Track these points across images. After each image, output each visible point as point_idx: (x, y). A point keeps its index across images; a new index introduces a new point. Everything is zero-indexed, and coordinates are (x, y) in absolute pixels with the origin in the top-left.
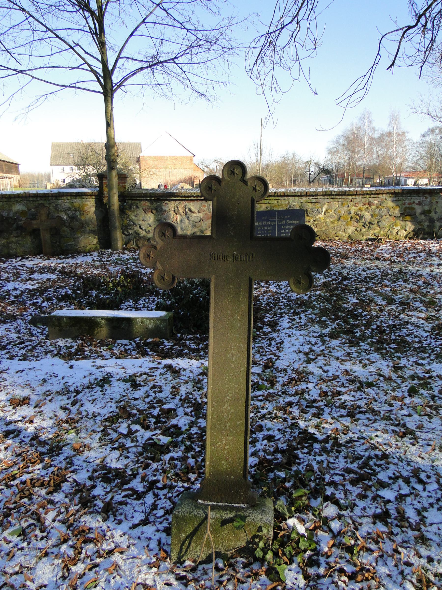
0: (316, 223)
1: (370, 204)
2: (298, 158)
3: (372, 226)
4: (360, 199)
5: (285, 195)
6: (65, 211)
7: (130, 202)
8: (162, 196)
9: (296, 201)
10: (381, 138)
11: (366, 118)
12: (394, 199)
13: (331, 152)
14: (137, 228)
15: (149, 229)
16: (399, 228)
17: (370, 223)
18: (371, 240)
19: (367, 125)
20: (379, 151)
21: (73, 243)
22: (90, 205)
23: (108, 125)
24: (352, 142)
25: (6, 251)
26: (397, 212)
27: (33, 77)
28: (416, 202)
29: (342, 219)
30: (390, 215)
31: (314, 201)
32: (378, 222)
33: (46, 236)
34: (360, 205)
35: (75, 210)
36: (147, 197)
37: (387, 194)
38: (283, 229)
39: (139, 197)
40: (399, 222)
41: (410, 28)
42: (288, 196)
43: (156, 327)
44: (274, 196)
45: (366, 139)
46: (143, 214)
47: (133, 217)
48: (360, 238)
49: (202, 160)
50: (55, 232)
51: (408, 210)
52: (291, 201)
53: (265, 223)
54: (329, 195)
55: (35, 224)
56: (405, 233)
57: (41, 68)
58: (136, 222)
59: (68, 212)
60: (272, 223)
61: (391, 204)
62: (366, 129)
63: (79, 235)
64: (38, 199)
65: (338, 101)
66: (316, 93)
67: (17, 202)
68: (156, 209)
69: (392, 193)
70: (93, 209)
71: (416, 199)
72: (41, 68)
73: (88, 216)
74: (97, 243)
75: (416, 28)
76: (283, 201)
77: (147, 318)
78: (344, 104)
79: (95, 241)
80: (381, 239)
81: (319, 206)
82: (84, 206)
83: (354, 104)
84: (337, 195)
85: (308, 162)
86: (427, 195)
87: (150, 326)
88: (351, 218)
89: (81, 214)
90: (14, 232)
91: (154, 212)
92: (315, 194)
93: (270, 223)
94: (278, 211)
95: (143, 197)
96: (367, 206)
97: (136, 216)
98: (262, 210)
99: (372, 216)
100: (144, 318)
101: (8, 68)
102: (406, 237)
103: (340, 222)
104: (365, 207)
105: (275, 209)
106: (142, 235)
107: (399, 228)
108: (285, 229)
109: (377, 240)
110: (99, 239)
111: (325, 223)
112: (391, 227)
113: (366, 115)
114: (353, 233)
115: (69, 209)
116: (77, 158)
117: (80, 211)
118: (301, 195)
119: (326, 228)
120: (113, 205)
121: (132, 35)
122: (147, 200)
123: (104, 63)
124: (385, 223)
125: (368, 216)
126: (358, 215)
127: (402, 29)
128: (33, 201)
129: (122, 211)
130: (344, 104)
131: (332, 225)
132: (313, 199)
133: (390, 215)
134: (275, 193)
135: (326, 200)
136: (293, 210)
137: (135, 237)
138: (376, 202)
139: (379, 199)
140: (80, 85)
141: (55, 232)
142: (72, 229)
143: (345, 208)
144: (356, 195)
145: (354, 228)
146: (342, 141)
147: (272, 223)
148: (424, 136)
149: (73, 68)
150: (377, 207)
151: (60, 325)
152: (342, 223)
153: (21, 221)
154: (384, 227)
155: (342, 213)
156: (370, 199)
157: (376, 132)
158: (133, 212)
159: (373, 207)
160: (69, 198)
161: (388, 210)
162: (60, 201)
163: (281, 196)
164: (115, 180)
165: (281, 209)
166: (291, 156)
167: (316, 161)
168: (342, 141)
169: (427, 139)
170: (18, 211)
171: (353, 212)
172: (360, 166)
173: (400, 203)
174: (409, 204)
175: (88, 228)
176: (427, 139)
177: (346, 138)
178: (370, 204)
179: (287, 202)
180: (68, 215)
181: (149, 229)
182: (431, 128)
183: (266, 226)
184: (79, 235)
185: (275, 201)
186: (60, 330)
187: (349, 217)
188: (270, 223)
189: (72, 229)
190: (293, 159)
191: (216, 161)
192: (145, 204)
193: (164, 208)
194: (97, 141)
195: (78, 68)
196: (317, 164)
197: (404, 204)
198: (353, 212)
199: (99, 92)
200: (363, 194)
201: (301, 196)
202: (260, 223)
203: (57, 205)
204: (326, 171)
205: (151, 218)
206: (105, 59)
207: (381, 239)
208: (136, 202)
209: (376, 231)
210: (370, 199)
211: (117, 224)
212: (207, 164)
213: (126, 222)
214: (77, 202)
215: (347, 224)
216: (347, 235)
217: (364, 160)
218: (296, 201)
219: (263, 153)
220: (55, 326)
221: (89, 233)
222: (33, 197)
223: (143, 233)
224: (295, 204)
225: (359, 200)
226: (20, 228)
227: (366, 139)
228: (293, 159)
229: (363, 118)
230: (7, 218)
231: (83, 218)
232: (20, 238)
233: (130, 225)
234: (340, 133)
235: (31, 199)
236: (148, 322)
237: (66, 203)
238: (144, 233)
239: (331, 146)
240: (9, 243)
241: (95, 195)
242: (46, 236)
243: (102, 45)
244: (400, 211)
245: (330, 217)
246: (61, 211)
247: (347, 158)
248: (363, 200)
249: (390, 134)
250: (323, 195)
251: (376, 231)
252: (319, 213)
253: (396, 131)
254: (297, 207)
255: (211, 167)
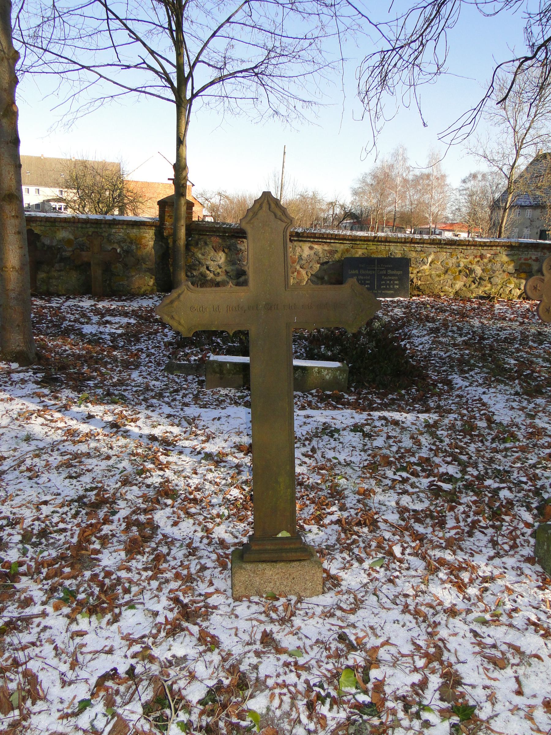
0: (419, 275)
1: (482, 257)
2: (319, 197)
3: (483, 283)
4: (471, 251)
5: (386, 240)
6: (119, 243)
7: (197, 237)
8: (238, 233)
9: (399, 248)
10: (417, 180)
11: (400, 155)
12: (510, 253)
13: (356, 193)
14: (203, 269)
15: (219, 270)
16: (512, 286)
17: (480, 278)
18: (482, 298)
19: (401, 163)
20: (412, 195)
21: (126, 283)
22: (149, 237)
23: (180, 142)
24: (382, 182)
25: (45, 288)
26: (511, 268)
27: (101, 76)
28: (534, 257)
29: (449, 272)
30: (504, 271)
31: (419, 249)
32: (489, 278)
33: (97, 272)
34: (471, 258)
35: (131, 243)
36: (219, 232)
37: (502, 246)
38: (383, 280)
39: (209, 231)
40: (513, 280)
41: (527, 59)
42: (390, 242)
43: (335, 378)
44: (373, 241)
45: (399, 180)
46: (212, 253)
47: (200, 256)
48: (469, 295)
49: (201, 191)
50: (107, 268)
51: (524, 267)
52: (392, 248)
53: (362, 272)
54: (437, 244)
55: (85, 256)
56: (519, 292)
57: (108, 65)
58: (203, 261)
59: (122, 245)
60: (370, 272)
61: (505, 259)
62: (399, 169)
63: (133, 274)
64: (88, 226)
65: (440, 136)
66: (424, 125)
67: (63, 227)
68: (229, 248)
69: (508, 246)
70: (151, 243)
71: (534, 254)
72: (108, 65)
73: (146, 250)
74: (154, 285)
75: (534, 60)
76: (383, 247)
77: (325, 368)
78: (448, 139)
79: (151, 282)
80: (494, 298)
81: (424, 255)
82: (142, 238)
83: (459, 140)
84: (445, 244)
85: (332, 203)
86: (545, 251)
87: (328, 377)
88: (460, 272)
89: (137, 248)
90: (57, 265)
91: (226, 250)
92: (422, 242)
93: (368, 272)
94: (378, 258)
95: (214, 232)
96: (478, 259)
97: (203, 255)
98: (357, 256)
99: (483, 270)
100: (322, 368)
101: (75, 63)
102: (519, 297)
103: (447, 276)
104: (476, 260)
105: (374, 256)
106: (209, 278)
107: (512, 286)
108: (385, 280)
109: (488, 297)
110: (156, 279)
111: (430, 275)
112: (505, 284)
113: (401, 151)
114: (460, 289)
115: (124, 241)
116: (64, 177)
117: (137, 245)
118: (405, 241)
119: (431, 281)
120: (180, 239)
121: (213, 35)
122: (219, 236)
123: (179, 67)
124: (498, 280)
125: (479, 271)
126: (468, 268)
127: (519, 59)
128: (82, 228)
129: (188, 246)
130: (448, 139)
131: (438, 279)
132: (418, 247)
133: (504, 271)
134: (375, 237)
135: (433, 249)
136: (395, 259)
137: (200, 280)
138: (488, 255)
139: (492, 252)
140: (147, 90)
141: (107, 268)
142: (125, 265)
143: (454, 260)
144: (468, 245)
145: (463, 283)
146: (369, 180)
147: (370, 272)
148: (464, 181)
149: (128, 67)
150: (490, 261)
151: (221, 372)
152: (448, 277)
153: (65, 251)
154: (497, 285)
155: (450, 265)
156: (483, 252)
157: (411, 173)
158: (201, 249)
159: (486, 260)
160: (125, 227)
161: (502, 265)
162: (114, 230)
163: (381, 242)
164: (183, 209)
165: (380, 256)
166: (311, 194)
167: (341, 203)
168: (369, 180)
169: (469, 185)
170: (63, 239)
171: (462, 265)
172: (390, 212)
173: (516, 257)
174: (526, 259)
175: (144, 266)
176: (469, 185)
177: (375, 177)
178: (482, 257)
179: (387, 248)
180: (122, 248)
181: (219, 270)
182: (473, 172)
183: (363, 275)
184: (133, 274)
185: (374, 247)
186: (221, 378)
187: (457, 270)
188: (368, 272)
189: (125, 265)
190: (314, 197)
191: (220, 194)
192: (216, 240)
193: (239, 246)
194: (46, 156)
195: (135, 66)
196: (343, 207)
197: (520, 259)
198: (462, 265)
199: (172, 101)
200: (475, 244)
201: (405, 242)
202: (357, 272)
203: (110, 235)
204: (349, 215)
205: (221, 258)
206: (181, 62)
207: (494, 298)
208: (205, 237)
209: (486, 289)
210: (483, 252)
211: (182, 263)
212: (208, 196)
213: (191, 261)
214: (134, 232)
215: (455, 279)
216: (454, 291)
217: (396, 204)
218: (399, 248)
219: (285, 188)
220: (216, 373)
221: (146, 271)
222: (94, 223)
223: (211, 276)
224: (397, 251)
225: (470, 251)
226: (63, 259)
227: (399, 180)
228: (314, 197)
229: (396, 155)
230: (50, 247)
231: (139, 253)
232: (63, 273)
233: (195, 265)
234: (368, 171)
235: (80, 225)
236: (326, 372)
237: (120, 233)
238: (212, 275)
239: (357, 186)
240: (49, 278)
241: (155, 226)
242: (97, 272)
243: (179, 44)
244: (514, 267)
245: (436, 269)
246: (114, 243)
247: (374, 201)
248: (475, 251)
249: (428, 176)
250: (430, 244)
251: (486, 289)
252: (424, 264)
253: (435, 174)
254: (399, 256)
255: (213, 201)
